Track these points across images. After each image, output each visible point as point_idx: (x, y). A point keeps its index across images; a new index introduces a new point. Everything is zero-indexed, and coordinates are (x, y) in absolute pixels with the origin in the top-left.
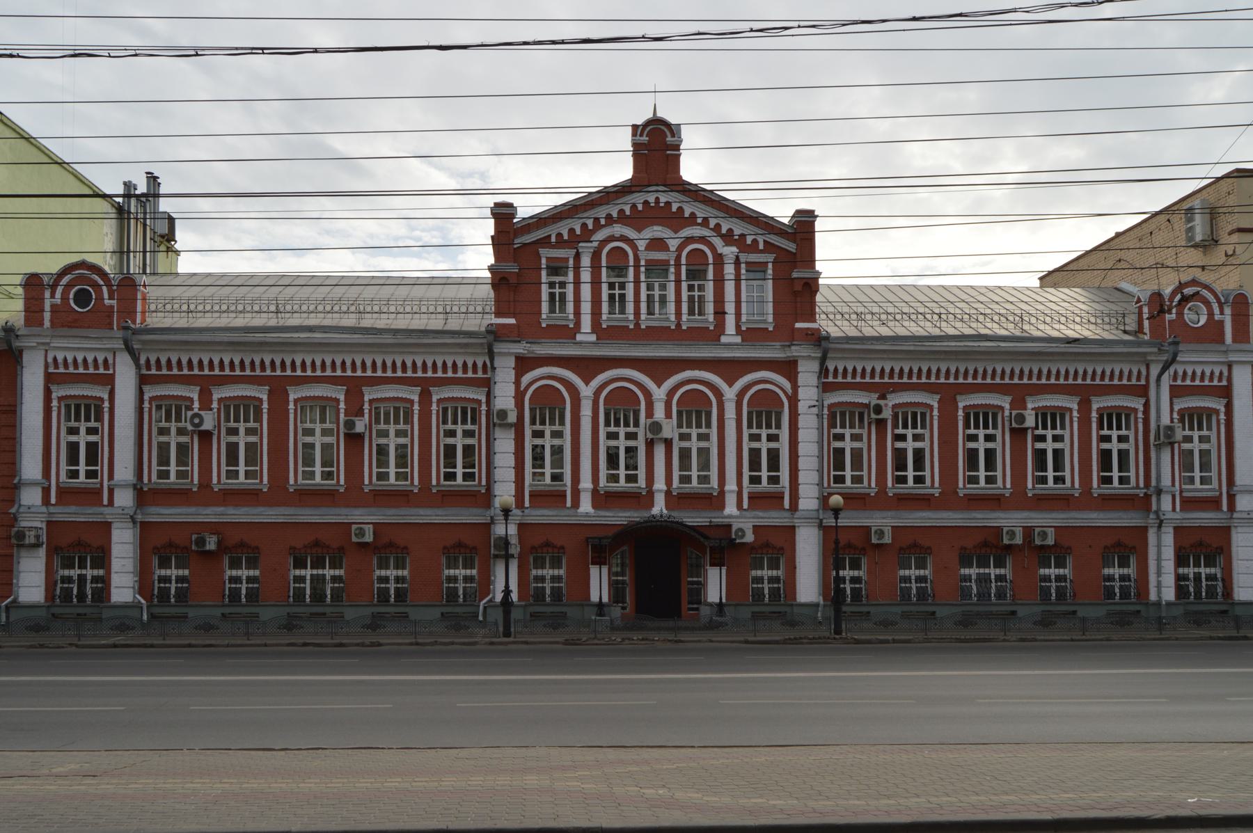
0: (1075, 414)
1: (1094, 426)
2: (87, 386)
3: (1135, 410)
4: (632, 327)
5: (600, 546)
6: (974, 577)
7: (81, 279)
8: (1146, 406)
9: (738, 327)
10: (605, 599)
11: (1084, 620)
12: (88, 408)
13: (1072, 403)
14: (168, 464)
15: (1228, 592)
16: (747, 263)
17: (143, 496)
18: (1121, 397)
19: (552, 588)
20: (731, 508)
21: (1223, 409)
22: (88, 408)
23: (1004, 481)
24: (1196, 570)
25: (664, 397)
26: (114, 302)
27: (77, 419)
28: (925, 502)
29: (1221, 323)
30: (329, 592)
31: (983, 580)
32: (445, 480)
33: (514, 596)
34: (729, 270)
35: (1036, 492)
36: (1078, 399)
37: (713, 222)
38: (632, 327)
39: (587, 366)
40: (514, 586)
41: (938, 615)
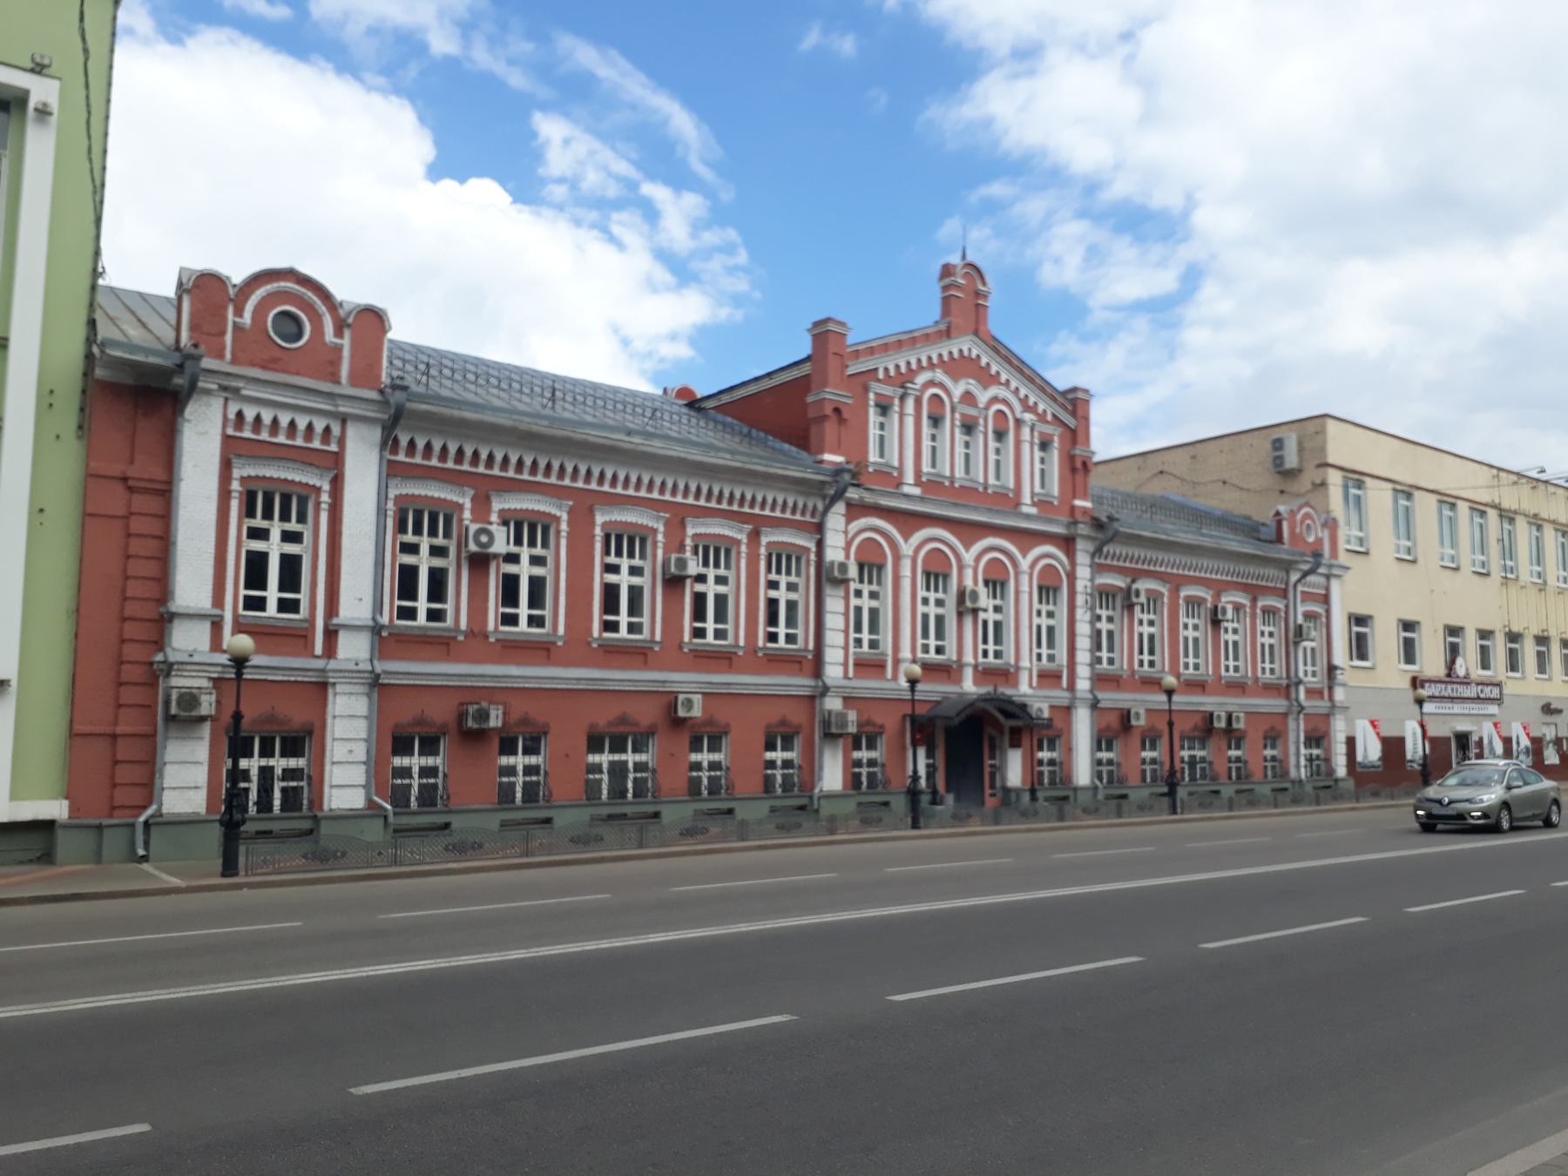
0: (660, 537)
1: (598, 547)
2: (538, 497)
4: (947, 483)
5: (923, 728)
6: (605, 766)
8: (1328, 611)
10: (1303, 776)
11: (832, 819)
12: (286, 500)
13: (740, 534)
14: (414, 597)
15: (316, 802)
16: (876, 394)
17: (385, 641)
18: (432, 483)
19: (710, 778)
20: (1024, 688)
21: (326, 487)
22: (286, 500)
23: (558, 622)
24: (264, 762)
25: (911, 553)
26: (346, 342)
27: (619, 553)
28: (542, 651)
30: (630, 785)
31: (618, 770)
32: (246, 607)
34: (1026, 432)
35: (500, 637)
36: (472, 492)
38: (947, 483)
39: (909, 520)
40: (922, 771)
41: (454, 826)
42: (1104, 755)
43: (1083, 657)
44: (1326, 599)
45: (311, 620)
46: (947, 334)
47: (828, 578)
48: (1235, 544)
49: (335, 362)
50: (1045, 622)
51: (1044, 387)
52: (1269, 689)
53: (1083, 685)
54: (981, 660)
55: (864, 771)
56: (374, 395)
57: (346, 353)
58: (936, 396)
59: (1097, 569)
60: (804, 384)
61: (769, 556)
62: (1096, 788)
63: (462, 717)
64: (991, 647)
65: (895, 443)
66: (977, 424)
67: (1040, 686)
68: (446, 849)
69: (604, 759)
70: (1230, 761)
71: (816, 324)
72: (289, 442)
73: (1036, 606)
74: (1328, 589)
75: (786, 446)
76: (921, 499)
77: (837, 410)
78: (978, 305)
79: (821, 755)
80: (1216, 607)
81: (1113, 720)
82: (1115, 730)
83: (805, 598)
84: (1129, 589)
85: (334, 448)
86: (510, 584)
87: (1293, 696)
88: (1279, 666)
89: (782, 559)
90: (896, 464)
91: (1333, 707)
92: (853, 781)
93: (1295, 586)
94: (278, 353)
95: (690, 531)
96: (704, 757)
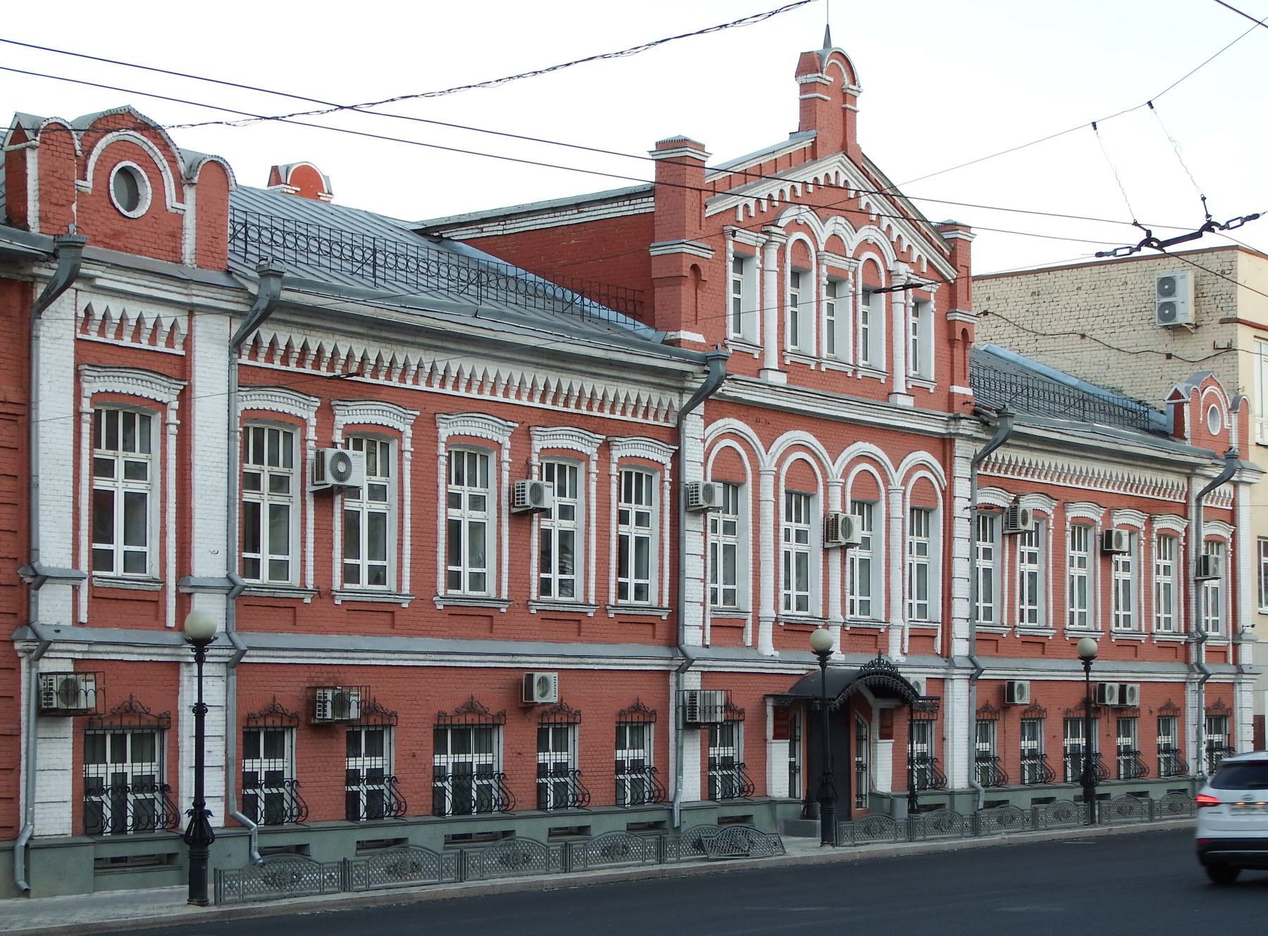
3: (163, 406)
7: (124, 149)
8: (185, 397)
9: (781, 357)
27: (259, 459)
28: (383, 615)
29: (179, 217)
33: (216, 820)
37: (885, 222)
39: (771, 419)
42: (260, 765)
43: (961, 609)
44: (1232, 518)
45: (163, 581)
46: (813, 154)
47: (684, 503)
48: (1134, 443)
49: (176, 235)
50: (794, 547)
51: (914, 219)
52: (634, 624)
53: (960, 648)
54: (783, 611)
55: (363, 789)
56: (222, 280)
57: (190, 222)
58: (800, 240)
59: (979, 481)
60: (644, 227)
61: (97, 415)
62: (977, 792)
63: (312, 704)
64: (631, 581)
65: (759, 311)
66: (845, 280)
67: (912, 651)
68: (501, 862)
69: (447, 760)
70: (1023, 758)
71: (662, 146)
72: (284, 368)
73: (784, 524)
74: (1234, 503)
75: (613, 315)
76: (788, 390)
77: (695, 268)
78: (845, 109)
79: (679, 748)
80: (1109, 533)
81: (990, 695)
82: (997, 705)
83: (656, 533)
84: (1014, 510)
85: (178, 350)
86: (351, 520)
87: (1193, 659)
88: (1176, 615)
89: (634, 481)
90: (758, 343)
91: (1240, 671)
92: (88, 818)
93: (1199, 500)
94: (119, 225)
95: (537, 445)
96: (362, 763)
